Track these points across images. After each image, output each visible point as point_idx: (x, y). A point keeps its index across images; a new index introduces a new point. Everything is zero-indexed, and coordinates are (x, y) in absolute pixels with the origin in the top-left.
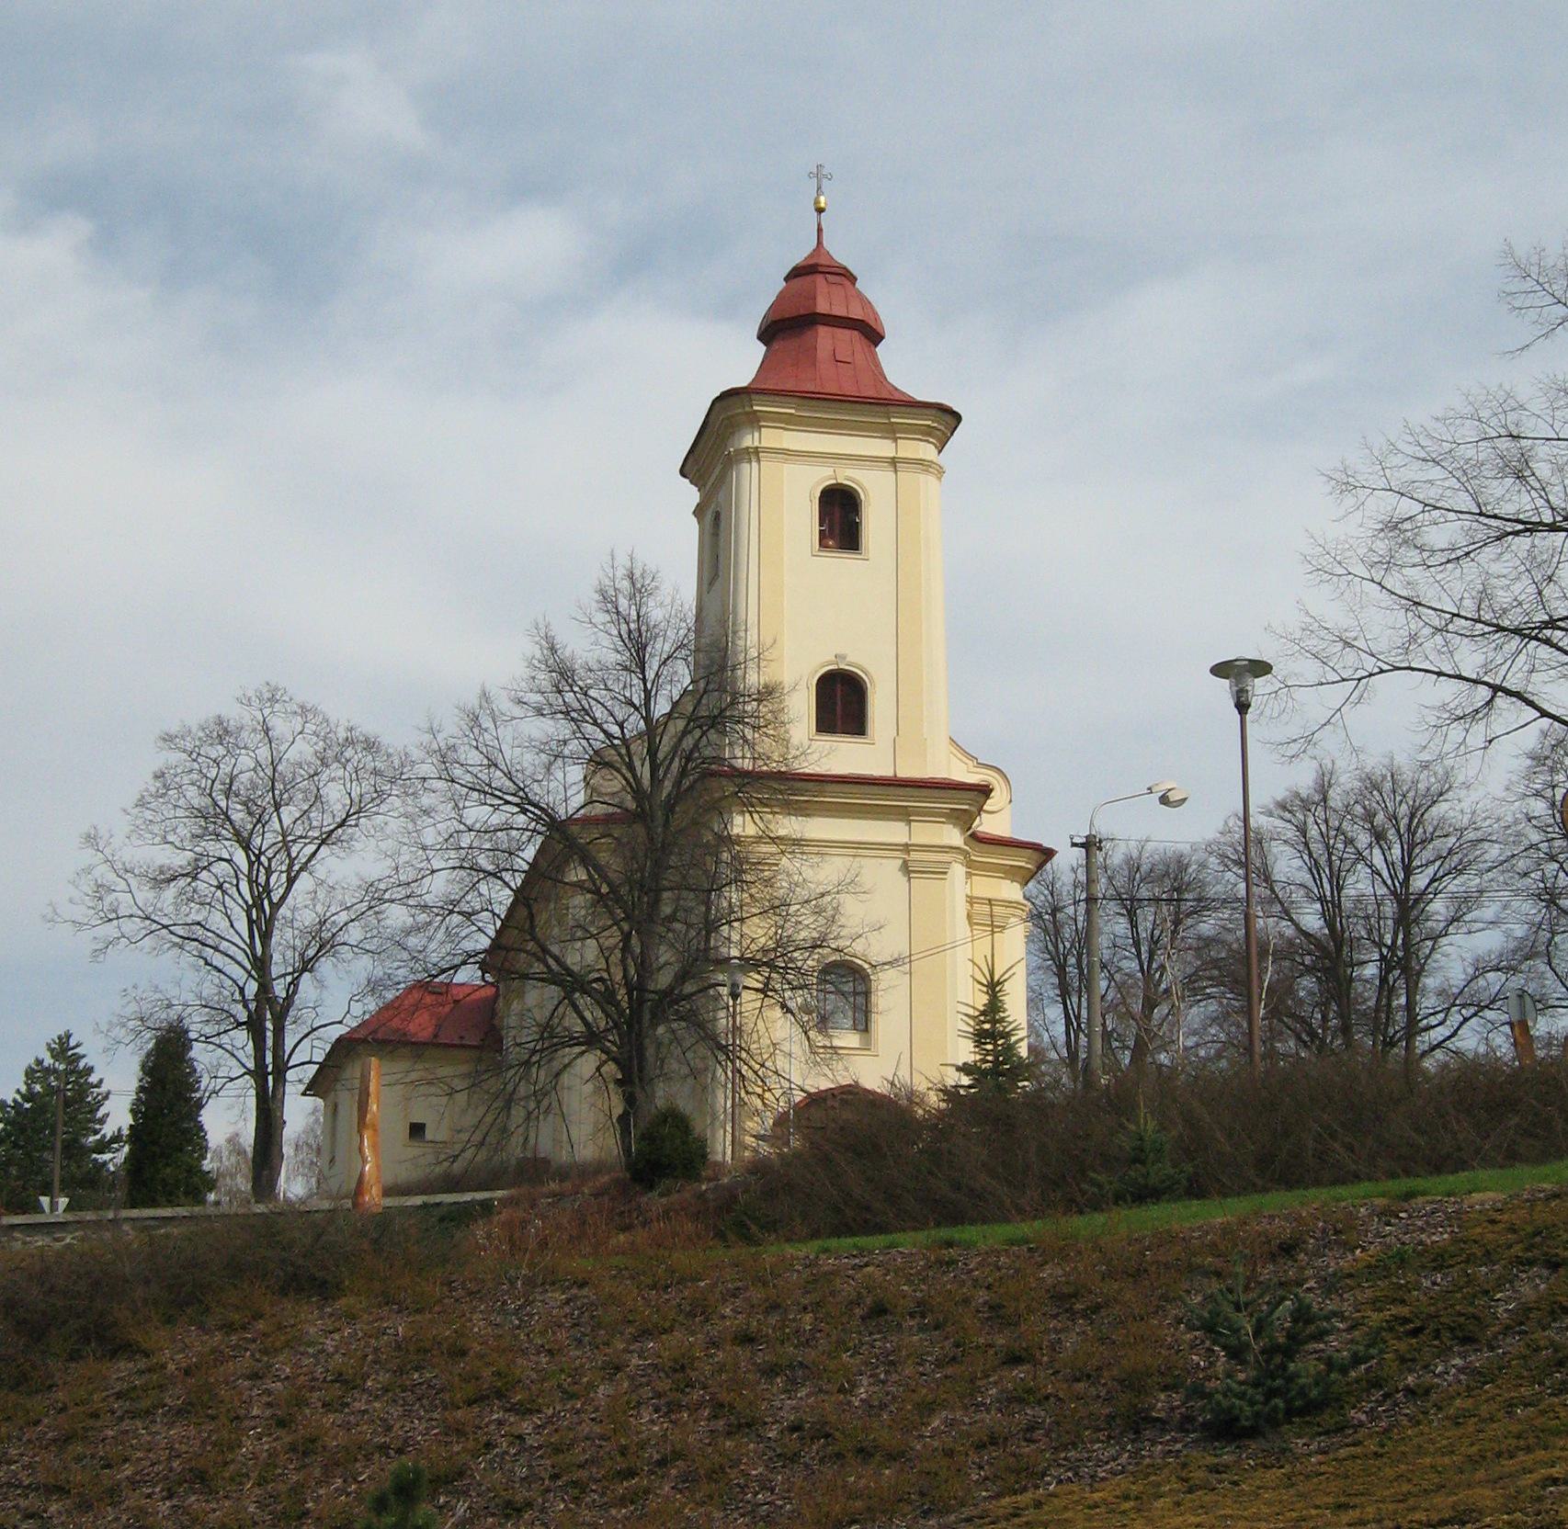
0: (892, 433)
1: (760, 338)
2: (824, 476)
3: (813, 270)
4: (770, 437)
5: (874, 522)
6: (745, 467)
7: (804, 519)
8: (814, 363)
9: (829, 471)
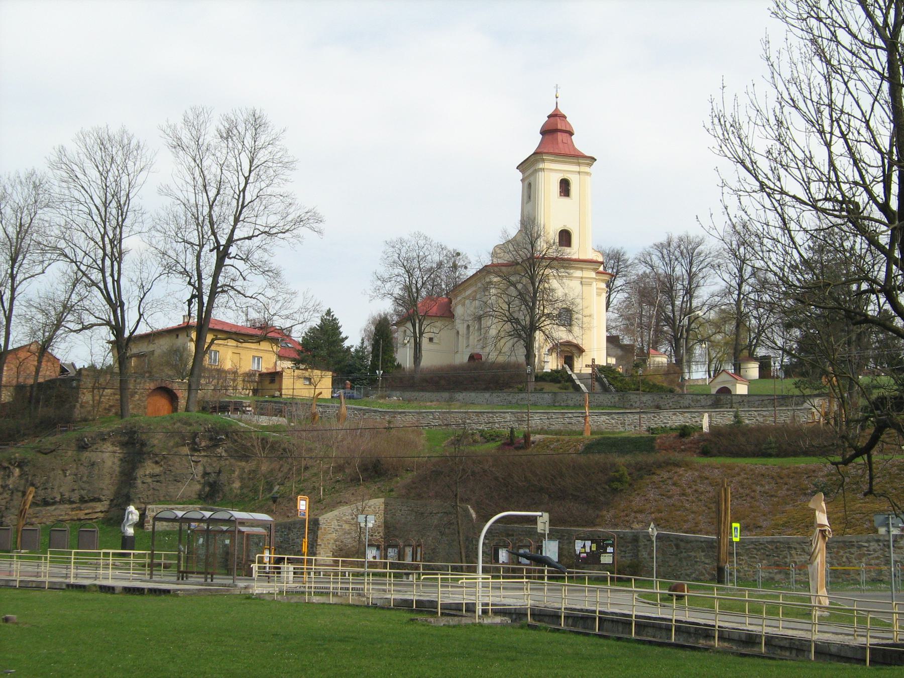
0: (579, 164)
1: (541, 133)
2: (561, 176)
3: (556, 115)
4: (547, 165)
5: (574, 189)
6: (540, 173)
7: (556, 188)
8: (557, 143)
9: (562, 175)
